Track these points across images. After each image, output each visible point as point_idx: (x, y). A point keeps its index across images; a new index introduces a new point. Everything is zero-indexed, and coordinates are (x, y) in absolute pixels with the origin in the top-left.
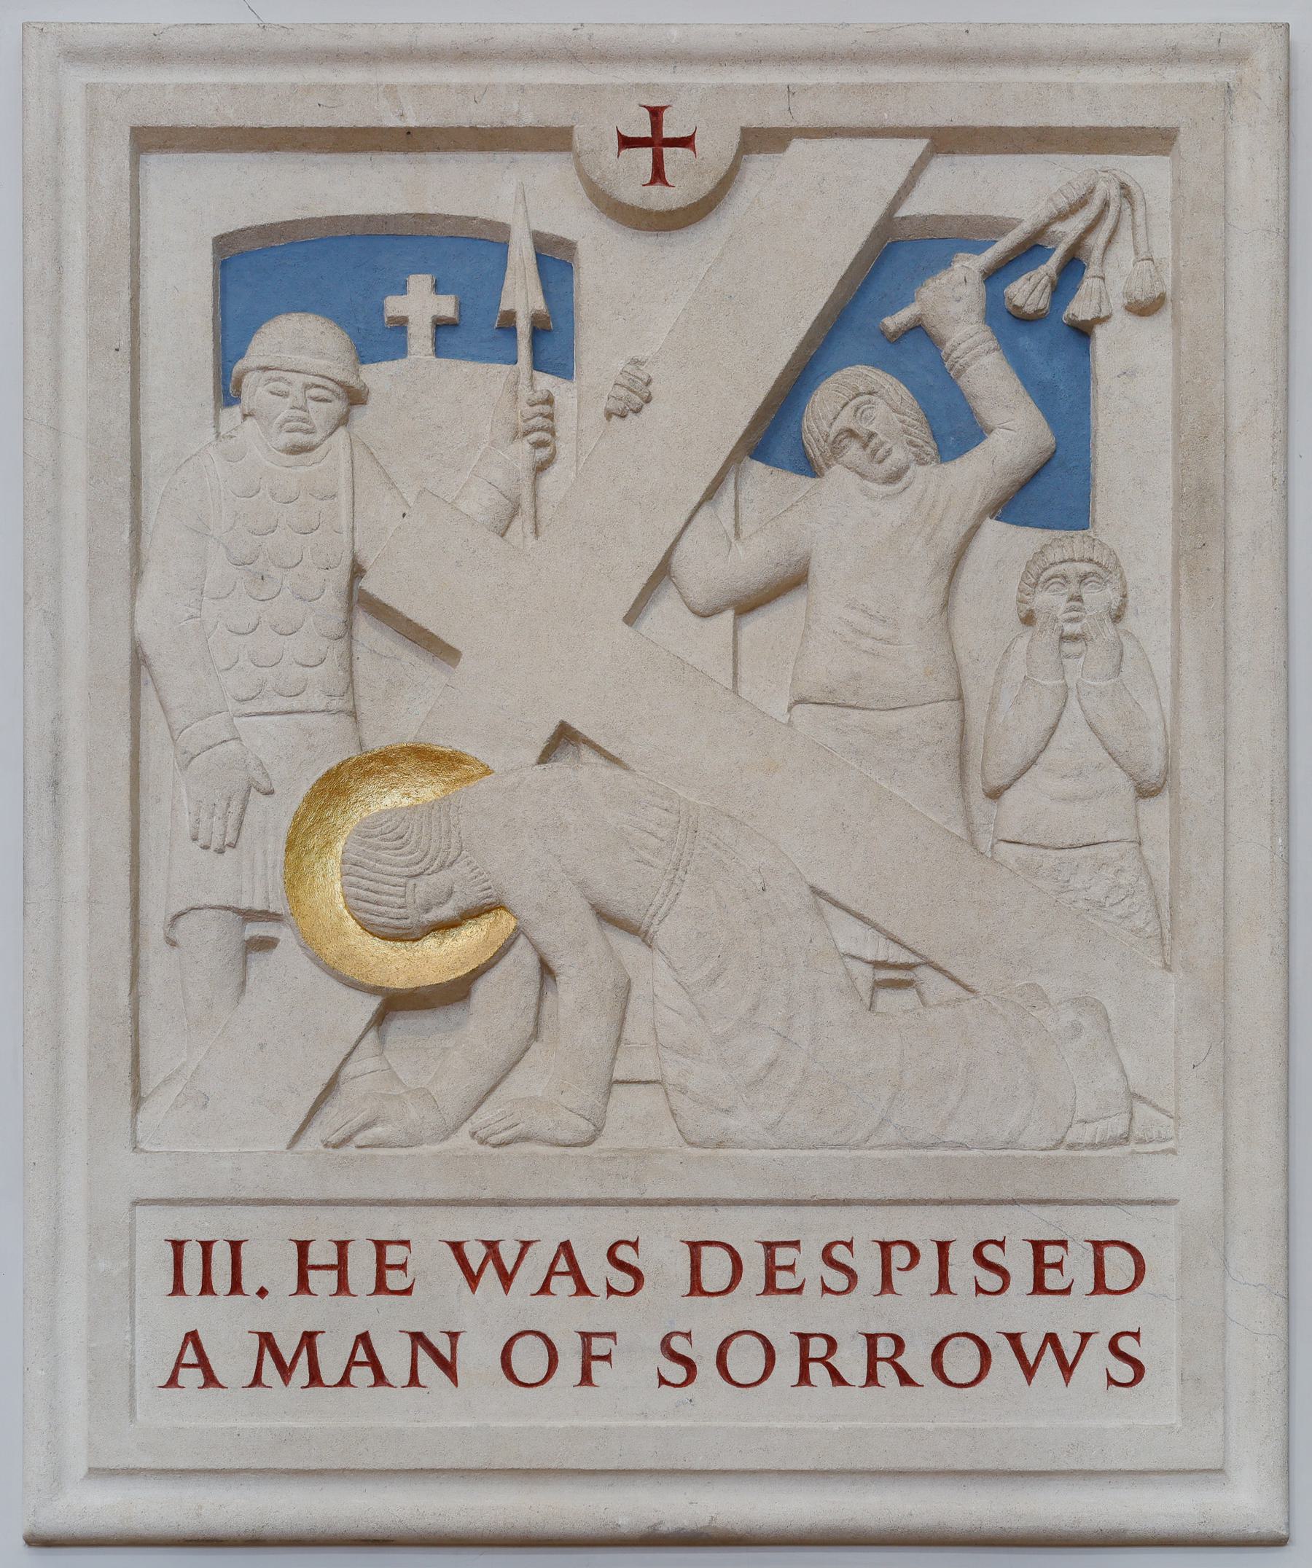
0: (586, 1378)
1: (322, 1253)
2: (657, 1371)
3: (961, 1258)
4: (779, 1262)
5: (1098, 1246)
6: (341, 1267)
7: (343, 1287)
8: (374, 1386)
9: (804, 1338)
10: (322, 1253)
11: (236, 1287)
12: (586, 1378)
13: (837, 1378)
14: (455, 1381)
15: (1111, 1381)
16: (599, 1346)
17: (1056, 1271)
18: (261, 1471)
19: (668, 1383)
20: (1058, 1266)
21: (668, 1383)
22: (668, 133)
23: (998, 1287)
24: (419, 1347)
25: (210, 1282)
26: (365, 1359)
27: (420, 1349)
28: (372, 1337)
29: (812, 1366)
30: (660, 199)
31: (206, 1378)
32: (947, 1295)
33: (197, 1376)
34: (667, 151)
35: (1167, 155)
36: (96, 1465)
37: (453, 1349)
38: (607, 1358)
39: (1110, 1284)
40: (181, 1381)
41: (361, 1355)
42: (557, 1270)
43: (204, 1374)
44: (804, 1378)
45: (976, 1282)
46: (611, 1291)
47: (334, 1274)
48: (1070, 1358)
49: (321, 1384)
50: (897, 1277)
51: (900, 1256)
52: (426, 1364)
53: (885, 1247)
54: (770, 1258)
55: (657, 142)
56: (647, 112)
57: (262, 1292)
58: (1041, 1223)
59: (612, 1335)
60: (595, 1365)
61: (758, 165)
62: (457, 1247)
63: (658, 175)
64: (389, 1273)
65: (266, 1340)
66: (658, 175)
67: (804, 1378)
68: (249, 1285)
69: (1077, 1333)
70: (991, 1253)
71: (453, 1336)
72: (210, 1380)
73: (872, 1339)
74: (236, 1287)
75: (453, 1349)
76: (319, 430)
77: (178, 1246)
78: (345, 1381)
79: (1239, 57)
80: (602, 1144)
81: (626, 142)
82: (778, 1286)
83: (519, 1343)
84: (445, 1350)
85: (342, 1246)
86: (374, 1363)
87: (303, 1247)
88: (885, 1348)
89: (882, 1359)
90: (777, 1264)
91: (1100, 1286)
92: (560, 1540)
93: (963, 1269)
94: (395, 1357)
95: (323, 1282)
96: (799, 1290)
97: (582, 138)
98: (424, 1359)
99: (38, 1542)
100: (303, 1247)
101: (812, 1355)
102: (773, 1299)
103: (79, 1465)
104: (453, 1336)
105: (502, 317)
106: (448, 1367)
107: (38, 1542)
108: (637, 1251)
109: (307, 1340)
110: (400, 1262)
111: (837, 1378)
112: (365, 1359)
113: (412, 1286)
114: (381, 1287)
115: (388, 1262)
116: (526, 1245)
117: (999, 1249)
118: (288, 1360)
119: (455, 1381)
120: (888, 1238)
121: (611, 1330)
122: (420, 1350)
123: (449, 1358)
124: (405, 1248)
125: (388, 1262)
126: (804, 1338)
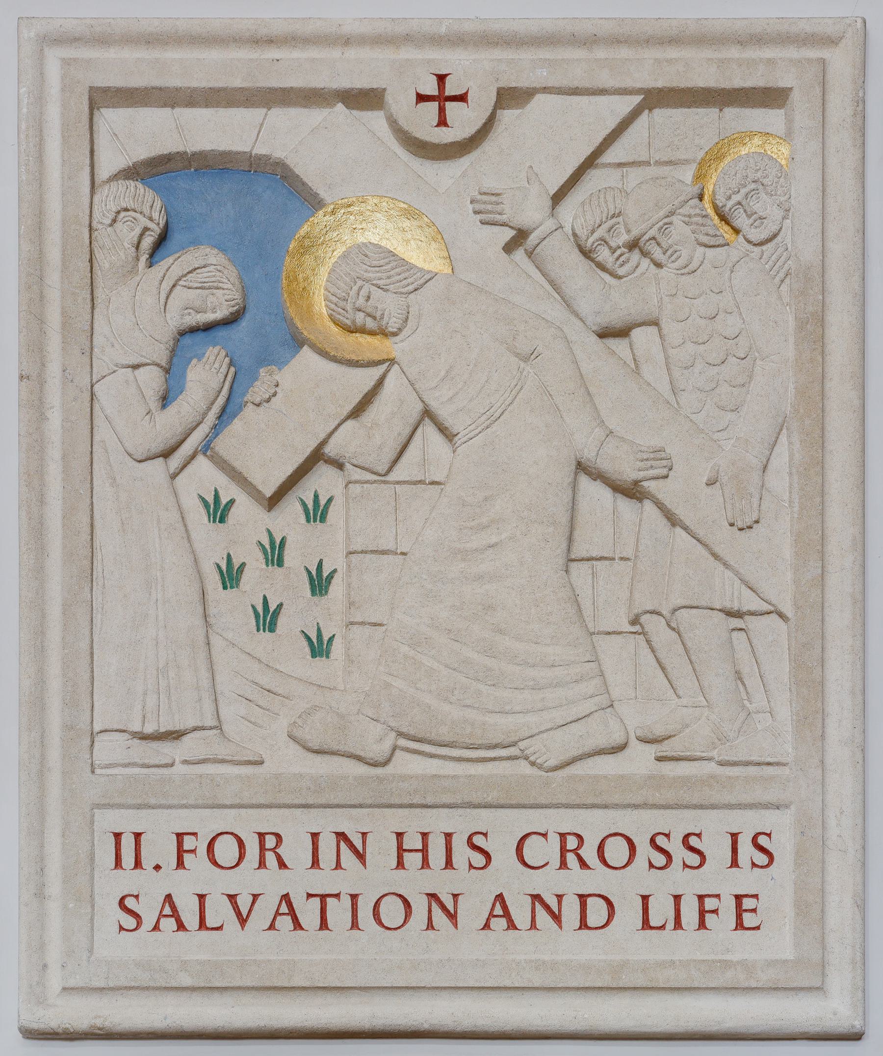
0: (702, 925)
1: (413, 841)
3: (327, 845)
4: (186, 848)
6: (424, 851)
7: (425, 864)
8: (177, 931)
9: (261, 836)
10: (413, 841)
11: (138, 864)
12: (702, 925)
13: (583, 864)
14: (561, 927)
15: (121, 928)
16: (710, 904)
18: (479, 988)
19: (124, 929)
21: (124, 929)
23: (766, 863)
24: (433, 902)
26: (501, 913)
27: (537, 903)
28: (291, 895)
30: (445, 136)
32: (402, 870)
33: (503, 922)
34: (449, 105)
35: (780, 107)
36: (67, 986)
38: (715, 912)
42: (164, 913)
44: (262, 864)
45: (470, 861)
46: (471, 866)
48: (244, 913)
52: (542, 915)
54: (180, 843)
55: (442, 99)
56: (435, 77)
57: (157, 868)
59: (756, 896)
60: (708, 916)
61: (507, 116)
62: (232, 898)
63: (442, 122)
66: (442, 122)
67: (262, 864)
68: (148, 862)
71: (455, 896)
72: (297, 925)
74: (138, 864)
77: (118, 836)
78: (156, 928)
79: (831, 41)
80: (389, 769)
81: (421, 98)
84: (450, 905)
86: (507, 914)
87: (400, 835)
92: (571, 1035)
93: (462, 853)
94: (521, 912)
95: (413, 860)
98: (437, 911)
99: (32, 1034)
100: (400, 835)
102: (204, 933)
103: (55, 981)
104: (455, 896)
106: (452, 917)
107: (32, 1034)
110: (193, 848)
111: (583, 864)
112: (501, 913)
114: (740, 925)
116: (255, 897)
117: (666, 839)
119: (561, 927)
120: (263, 831)
121: (756, 893)
123: (557, 913)
125: (707, 908)
126: (261, 836)
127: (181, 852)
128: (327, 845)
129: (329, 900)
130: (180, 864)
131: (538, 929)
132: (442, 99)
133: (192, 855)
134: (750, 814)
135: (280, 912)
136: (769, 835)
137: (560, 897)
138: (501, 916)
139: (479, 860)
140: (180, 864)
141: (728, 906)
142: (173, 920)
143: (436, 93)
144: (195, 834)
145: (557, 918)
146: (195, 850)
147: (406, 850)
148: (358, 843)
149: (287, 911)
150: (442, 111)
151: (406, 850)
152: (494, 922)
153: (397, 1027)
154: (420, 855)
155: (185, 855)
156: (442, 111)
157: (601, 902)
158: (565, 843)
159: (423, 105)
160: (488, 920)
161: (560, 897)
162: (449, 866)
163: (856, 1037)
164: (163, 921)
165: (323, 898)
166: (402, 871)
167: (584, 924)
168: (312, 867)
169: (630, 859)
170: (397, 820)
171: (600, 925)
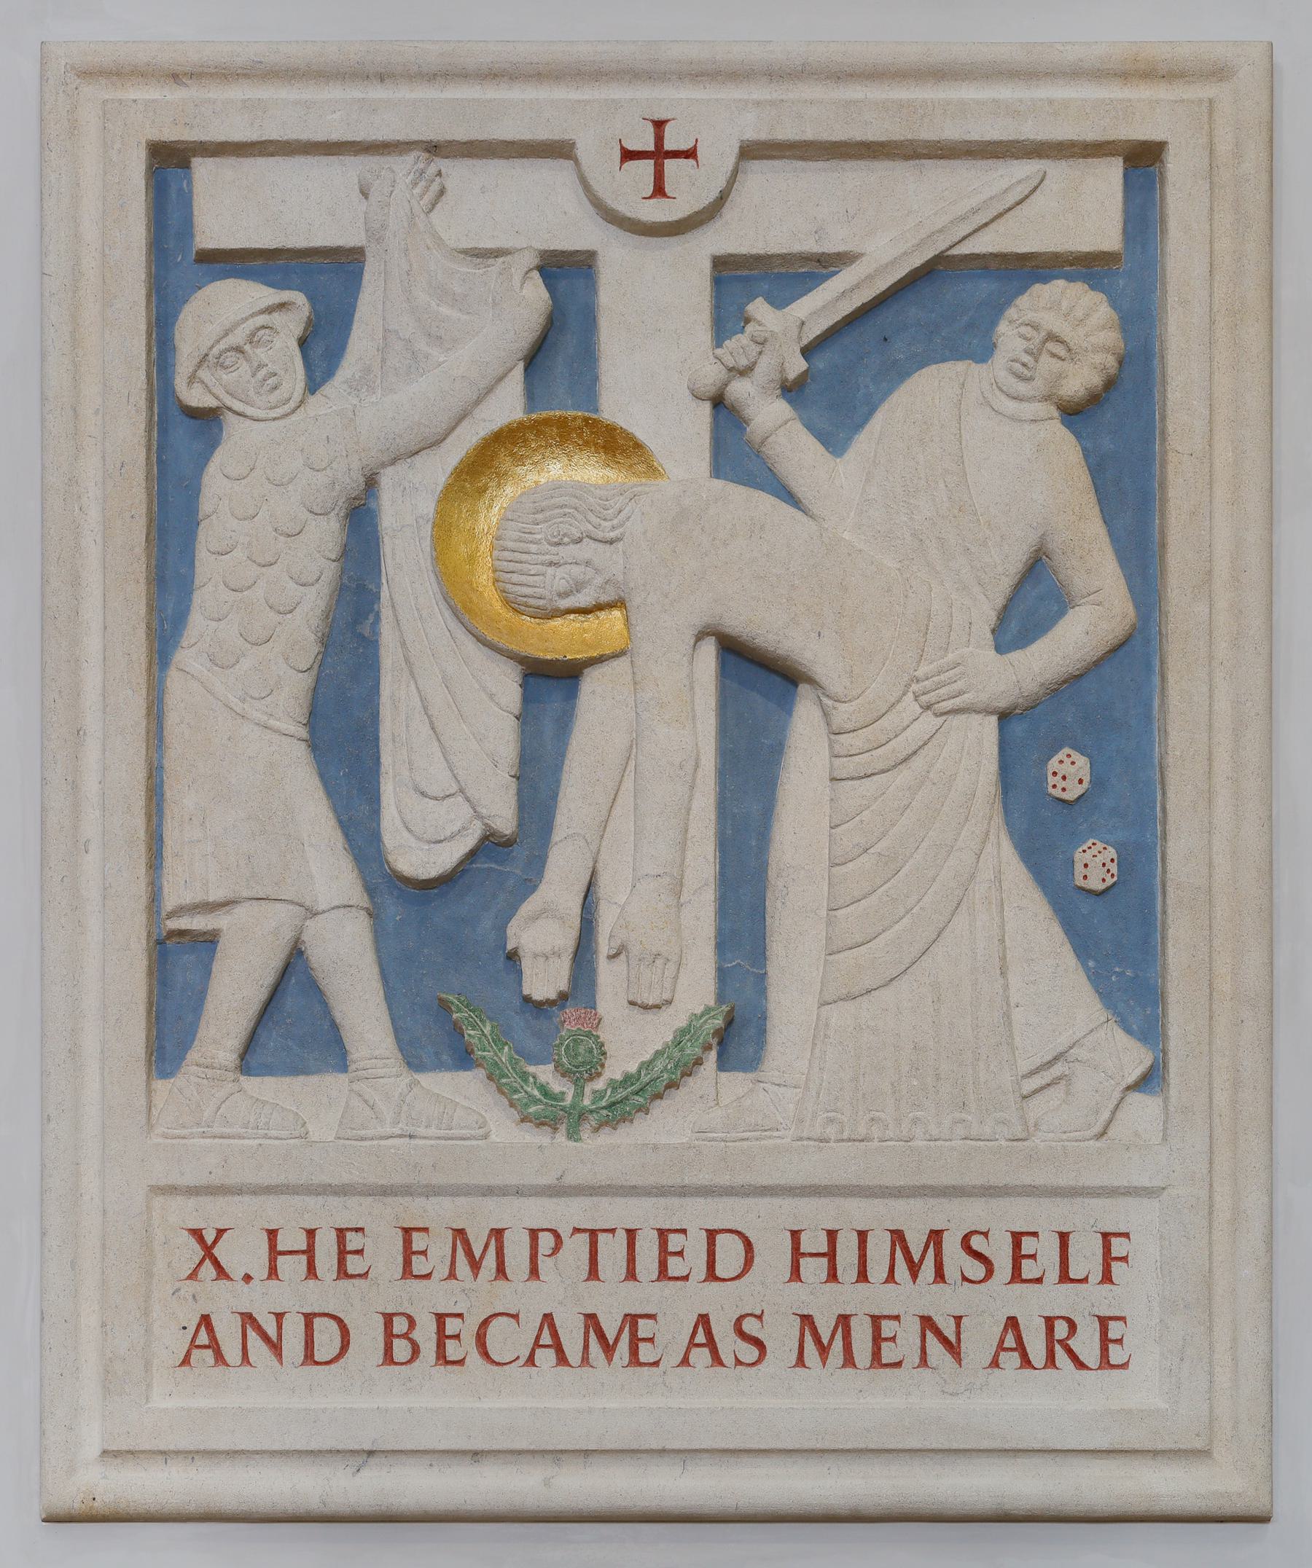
1: (814, 1241)
2: (733, 1356)
5: (712, 1235)
6: (831, 1255)
9: (1050, 1322)
14: (824, 1365)
17: (422, 1258)
20: (359, 1252)
22: (669, 146)
25: (634, 1269)
26: (704, 1341)
29: (396, 1342)
31: (558, 1359)
34: (670, 164)
37: (280, 1327)
39: (719, 1272)
40: (692, 1360)
41: (546, 1338)
42: (1006, 1345)
43: (557, 1355)
47: (825, 1261)
49: (721, 1364)
50: (543, 1264)
51: (546, 1241)
53: (534, 1234)
54: (407, 1242)
57: (247, 1278)
58: (1019, 1214)
63: (659, 190)
64: (642, 1346)
65: (807, 1320)
66: (659, 190)
69: (797, 1314)
70: (976, 1243)
73: (388, 1318)
75: (280, 1327)
76: (1038, 383)
82: (1024, 1276)
83: (495, 1323)
85: (832, 1235)
86: (1021, 1348)
87: (795, 1235)
88: (1061, 1330)
89: (398, 1336)
90: (348, 1248)
91: (711, 1275)
95: (814, 1269)
96: (1039, 1281)
97: (584, 151)
101: (395, 1331)
102: (1017, 1287)
104: (958, 1319)
105: (197, 252)
106: (953, 1348)
107: (51, 1519)
108: (226, 1230)
109: (205, 1320)
113: (431, 1273)
114: (663, 1273)
115: (280, 1248)
118: (611, 1339)
119: (824, 1365)
122: (929, 1335)
124: (682, 1236)
125: (280, 1248)
127: (1108, 1258)
128: (879, 1249)
129: (602, 1238)
130: (1107, 1278)
131: (592, 1367)
132: (659, 154)
133: (649, 1345)
134: (700, 1203)
135: (541, 1343)
136: (986, 1234)
137: (279, 1317)
138: (1011, 1350)
139: (750, 1353)
140: (1107, 1278)
141: (426, 1334)
142: (1016, 1354)
143: (651, 148)
144: (684, 1231)
145: (276, 1347)
146: (362, 1250)
147: (823, 1255)
148: (950, 1333)
149: (704, 1341)
150: (659, 139)
151: (804, 1255)
152: (1003, 1356)
153: (979, 1512)
154: (825, 1261)
155: (414, 1258)
156: (659, 139)
157: (333, 1325)
158: (411, 1243)
159: (632, 165)
160: (533, 1351)
161: (279, 1317)
162: (938, 1279)
163: (1264, 1519)
164: (196, 1354)
165: (593, 1233)
166: (275, 1282)
167: (309, 1358)
168: (269, 1277)
169: (745, 1264)
170: (274, 1211)
171: (751, 1362)
